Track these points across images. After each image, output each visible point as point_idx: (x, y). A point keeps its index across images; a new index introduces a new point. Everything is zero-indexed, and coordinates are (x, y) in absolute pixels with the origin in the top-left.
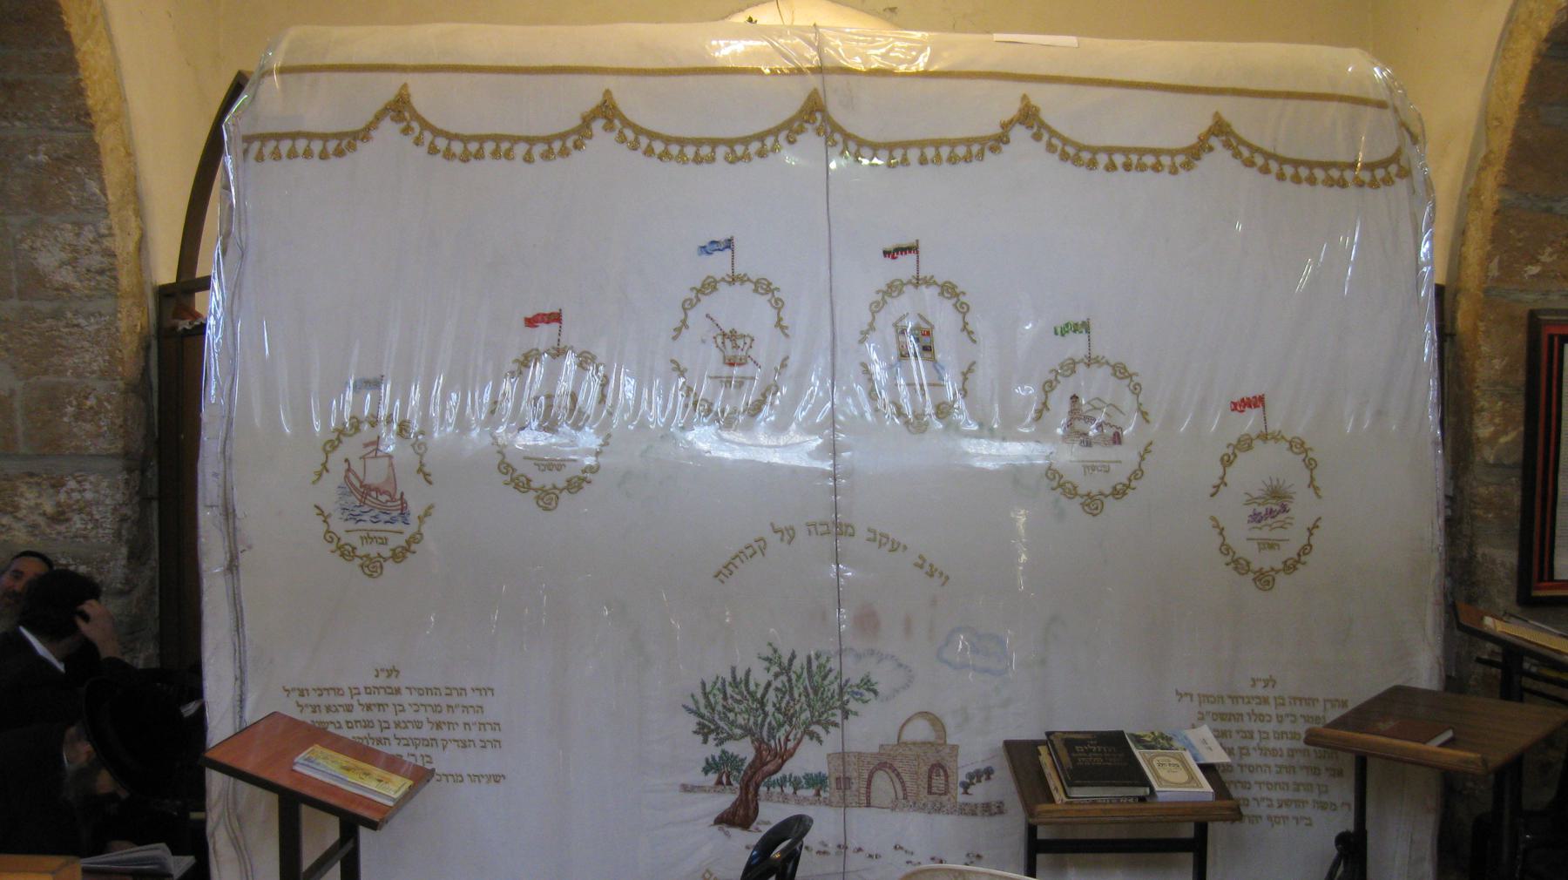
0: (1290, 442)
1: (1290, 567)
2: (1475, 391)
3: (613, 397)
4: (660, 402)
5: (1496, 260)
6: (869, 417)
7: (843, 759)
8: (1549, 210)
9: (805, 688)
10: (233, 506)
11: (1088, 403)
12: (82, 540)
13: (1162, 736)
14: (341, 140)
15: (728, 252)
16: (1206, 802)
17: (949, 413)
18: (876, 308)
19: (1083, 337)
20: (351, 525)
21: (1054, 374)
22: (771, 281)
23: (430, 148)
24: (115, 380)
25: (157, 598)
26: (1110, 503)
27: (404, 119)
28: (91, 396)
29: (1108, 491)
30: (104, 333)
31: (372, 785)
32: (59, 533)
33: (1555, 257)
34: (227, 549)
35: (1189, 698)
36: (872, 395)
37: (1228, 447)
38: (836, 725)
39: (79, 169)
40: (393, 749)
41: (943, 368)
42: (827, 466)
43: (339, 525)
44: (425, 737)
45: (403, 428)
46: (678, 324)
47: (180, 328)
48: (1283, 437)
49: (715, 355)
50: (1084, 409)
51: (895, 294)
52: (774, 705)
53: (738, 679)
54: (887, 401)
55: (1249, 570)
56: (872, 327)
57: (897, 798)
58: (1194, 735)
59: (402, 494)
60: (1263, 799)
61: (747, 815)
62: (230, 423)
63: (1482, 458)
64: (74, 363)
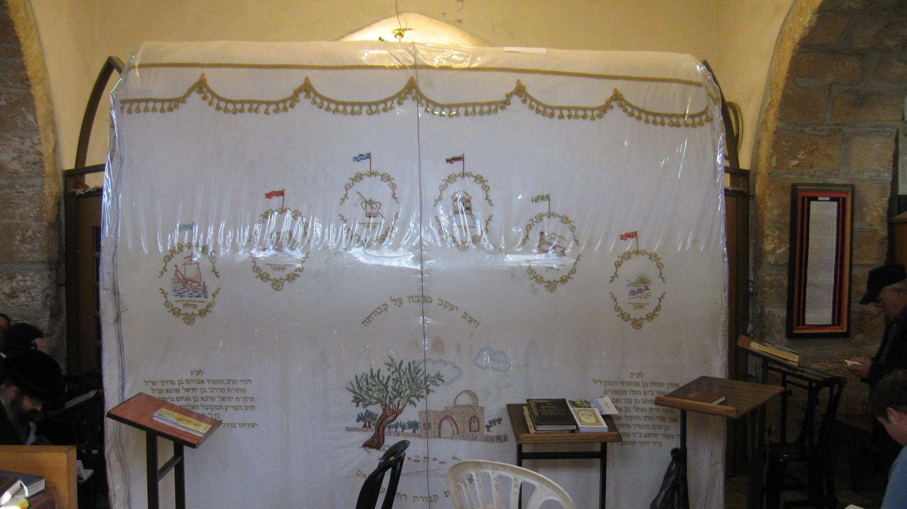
0: (650, 255)
1: (650, 317)
2: (764, 226)
3: (310, 233)
4: (334, 236)
5: (775, 158)
6: (439, 243)
7: (427, 414)
8: (802, 131)
9: (408, 378)
10: (118, 289)
11: (549, 235)
12: (25, 307)
13: (585, 401)
14: (171, 103)
15: (368, 160)
16: (604, 433)
17: (479, 241)
18: (443, 188)
19: (546, 203)
20: (178, 298)
21: (531, 221)
22: (389, 175)
23: (217, 107)
24: (42, 221)
25: (65, 338)
26: (559, 285)
27: (203, 92)
28: (30, 230)
29: (558, 279)
30: (36, 196)
31: (191, 426)
32: (12, 304)
33: (806, 156)
34: (115, 311)
35: (599, 383)
36: (440, 232)
37: (618, 257)
38: (423, 397)
39: (23, 109)
40: (201, 411)
41: (476, 218)
42: (418, 268)
43: (172, 298)
44: (216, 405)
45: (205, 249)
46: (343, 196)
47: (77, 194)
48: (646, 253)
49: (362, 212)
50: (546, 239)
51: (452, 181)
52: (392, 387)
53: (374, 375)
54: (448, 235)
55: (629, 319)
56: (440, 198)
57: (454, 433)
58: (601, 401)
59: (204, 283)
60: (637, 433)
61: (379, 442)
62: (116, 247)
63: (768, 261)
64: (21, 212)
